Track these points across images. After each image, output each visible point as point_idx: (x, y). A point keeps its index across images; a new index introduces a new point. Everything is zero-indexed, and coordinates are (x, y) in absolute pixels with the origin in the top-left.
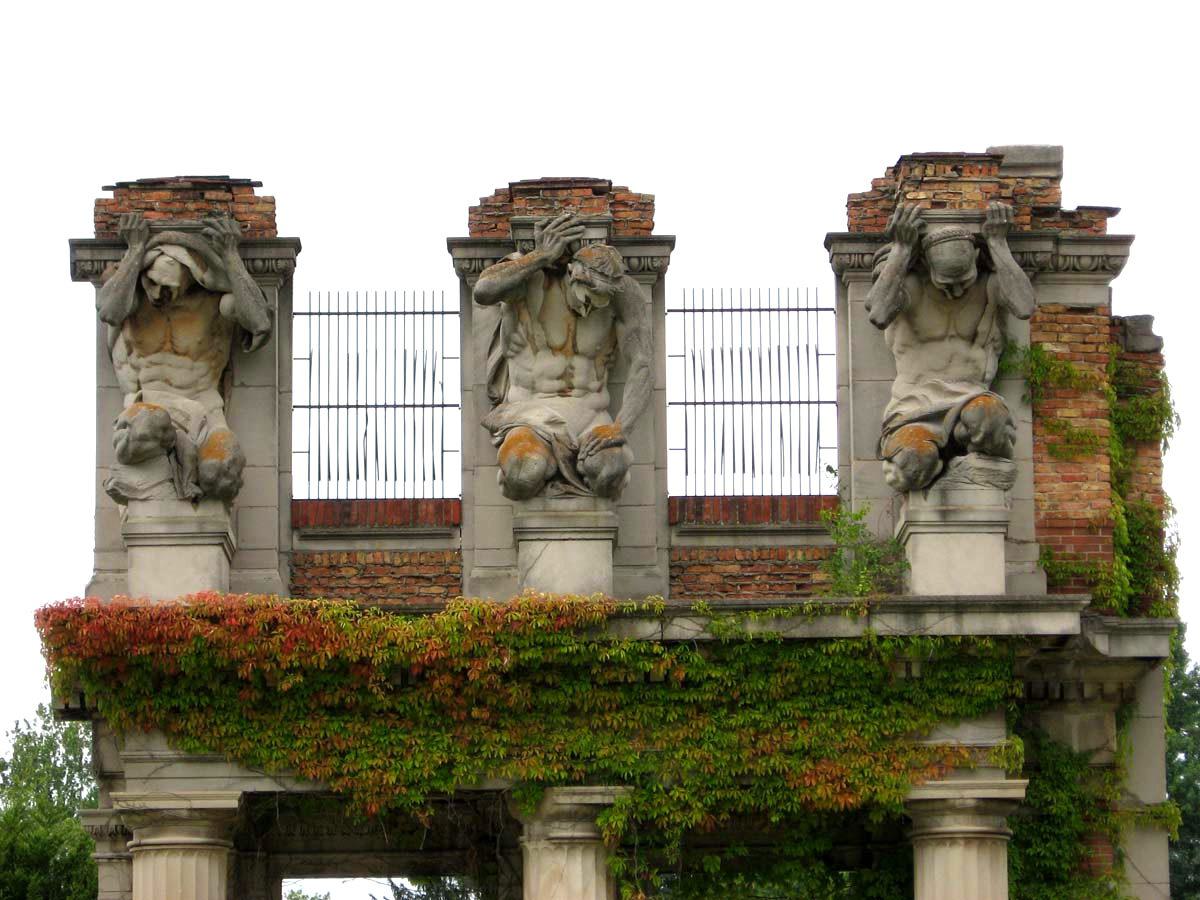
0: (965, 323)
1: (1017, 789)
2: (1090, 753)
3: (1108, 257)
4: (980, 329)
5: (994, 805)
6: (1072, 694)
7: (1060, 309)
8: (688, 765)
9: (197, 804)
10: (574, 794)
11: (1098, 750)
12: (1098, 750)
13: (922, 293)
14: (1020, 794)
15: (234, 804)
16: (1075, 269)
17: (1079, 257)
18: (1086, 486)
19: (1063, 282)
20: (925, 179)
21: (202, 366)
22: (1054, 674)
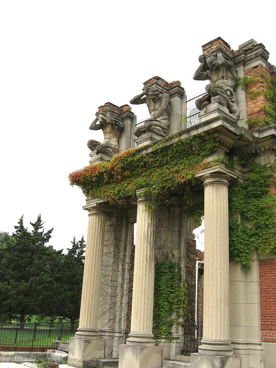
0: (220, 76)
2: (266, 165)
3: (257, 53)
4: (223, 75)
5: (214, 174)
6: (259, 152)
7: (251, 69)
8: (156, 179)
9: (92, 206)
10: (139, 191)
11: (268, 164)
12: (268, 164)
13: (212, 73)
15: (95, 205)
16: (252, 59)
17: (252, 56)
18: (258, 103)
19: (249, 64)
20: (215, 54)
21: (111, 135)
22: (251, 147)
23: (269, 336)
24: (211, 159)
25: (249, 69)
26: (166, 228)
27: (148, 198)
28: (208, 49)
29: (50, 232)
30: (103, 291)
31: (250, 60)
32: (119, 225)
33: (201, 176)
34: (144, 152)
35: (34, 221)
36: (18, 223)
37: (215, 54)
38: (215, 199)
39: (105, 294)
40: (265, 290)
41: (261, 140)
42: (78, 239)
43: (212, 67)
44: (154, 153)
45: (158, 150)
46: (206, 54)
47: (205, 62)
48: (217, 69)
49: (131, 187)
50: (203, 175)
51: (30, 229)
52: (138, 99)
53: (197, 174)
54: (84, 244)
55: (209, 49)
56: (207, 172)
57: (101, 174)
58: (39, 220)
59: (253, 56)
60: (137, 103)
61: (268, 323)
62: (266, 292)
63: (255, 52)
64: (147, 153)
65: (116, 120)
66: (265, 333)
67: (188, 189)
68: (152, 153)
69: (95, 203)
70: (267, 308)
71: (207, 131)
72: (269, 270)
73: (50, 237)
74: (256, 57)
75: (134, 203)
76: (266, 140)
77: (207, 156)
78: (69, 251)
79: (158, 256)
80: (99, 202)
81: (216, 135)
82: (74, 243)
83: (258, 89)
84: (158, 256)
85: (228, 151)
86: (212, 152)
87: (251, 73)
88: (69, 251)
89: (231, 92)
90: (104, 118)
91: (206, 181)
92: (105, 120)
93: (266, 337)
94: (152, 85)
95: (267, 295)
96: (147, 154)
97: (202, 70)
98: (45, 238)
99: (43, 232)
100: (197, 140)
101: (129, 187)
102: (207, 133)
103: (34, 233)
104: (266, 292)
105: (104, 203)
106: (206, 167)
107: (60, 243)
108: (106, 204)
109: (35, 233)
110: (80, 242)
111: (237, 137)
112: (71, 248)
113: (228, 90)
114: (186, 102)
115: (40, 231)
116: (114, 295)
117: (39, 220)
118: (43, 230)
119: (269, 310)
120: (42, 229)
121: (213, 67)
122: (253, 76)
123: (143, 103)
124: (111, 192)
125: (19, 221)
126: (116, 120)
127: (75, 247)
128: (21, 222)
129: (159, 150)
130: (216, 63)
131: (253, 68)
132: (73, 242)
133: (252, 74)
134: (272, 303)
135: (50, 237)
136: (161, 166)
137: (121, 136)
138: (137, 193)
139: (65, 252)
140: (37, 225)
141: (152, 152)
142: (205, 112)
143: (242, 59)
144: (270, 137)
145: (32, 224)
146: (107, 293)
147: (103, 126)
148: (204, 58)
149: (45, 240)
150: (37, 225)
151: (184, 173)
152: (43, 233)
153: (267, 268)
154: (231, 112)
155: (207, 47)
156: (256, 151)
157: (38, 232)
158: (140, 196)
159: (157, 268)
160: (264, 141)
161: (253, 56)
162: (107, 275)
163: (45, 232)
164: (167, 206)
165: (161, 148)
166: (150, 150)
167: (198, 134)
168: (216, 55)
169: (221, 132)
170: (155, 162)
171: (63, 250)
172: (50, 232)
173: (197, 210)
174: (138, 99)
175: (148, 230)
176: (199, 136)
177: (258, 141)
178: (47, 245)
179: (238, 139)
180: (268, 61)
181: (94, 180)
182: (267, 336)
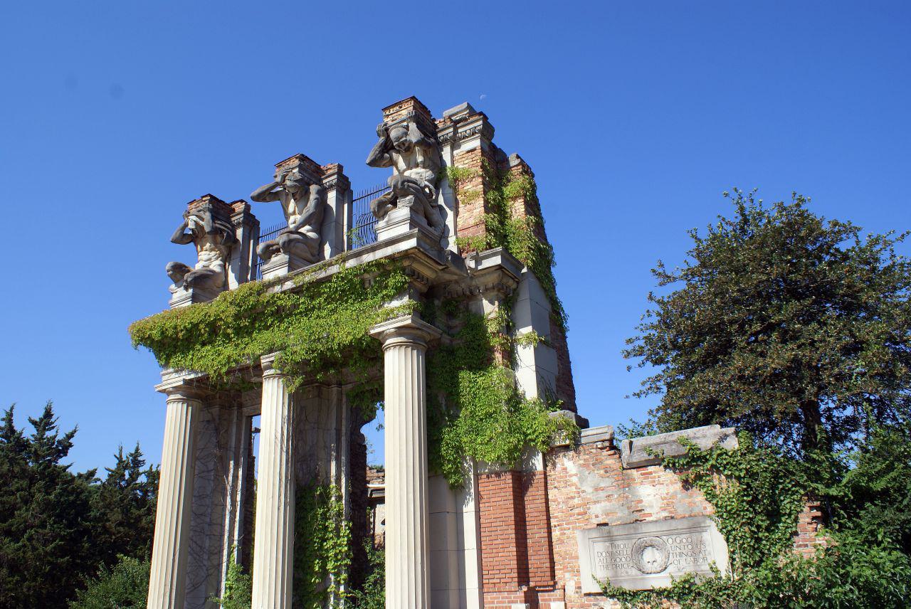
1: (407, 321)
3: (475, 127)
5: (403, 331)
8: (297, 338)
14: (409, 322)
17: (466, 131)
18: (475, 211)
20: (405, 124)
23: (498, 602)
24: (395, 304)
25: (461, 153)
26: (315, 423)
27: (286, 373)
28: (393, 115)
29: (71, 436)
30: (194, 545)
31: (464, 138)
32: (225, 420)
33: (380, 333)
34: (277, 289)
35: (38, 415)
36: (3, 419)
37: (405, 124)
38: (401, 373)
39: (198, 549)
40: (489, 525)
41: (481, 273)
42: (128, 450)
43: (399, 146)
44: (296, 291)
45: (302, 286)
46: (390, 123)
47: (388, 136)
48: (409, 150)
49: (254, 348)
50: (383, 332)
51: (29, 432)
52: (267, 193)
53: (373, 328)
54: (140, 458)
55: (396, 114)
56: (389, 327)
57: (195, 326)
58: (48, 414)
59: (468, 132)
60: (264, 200)
61: (495, 581)
62: (490, 529)
63: (471, 126)
64: (283, 289)
65: (223, 227)
66: (491, 598)
67: (356, 355)
68: (293, 291)
69: (182, 378)
70: (493, 555)
71: (391, 255)
72: (494, 492)
73: (71, 445)
74: (473, 135)
75: (254, 380)
76: (488, 273)
77: (391, 298)
78: (110, 473)
79: (301, 475)
80: (188, 377)
81: (406, 263)
82: (120, 459)
83: (475, 188)
84: (301, 475)
85: (425, 289)
86: (399, 292)
87: (464, 159)
88: (110, 473)
89: (430, 190)
90: (201, 223)
91: (388, 342)
92: (202, 227)
93: (491, 605)
94: (293, 169)
95: (493, 533)
96: (284, 292)
97: (383, 150)
98: (60, 448)
99: (55, 436)
100: (374, 269)
101: (253, 347)
102: (392, 258)
103: (36, 439)
104: (490, 529)
105: (198, 380)
106: (388, 316)
107: (89, 459)
108: (201, 382)
109: (40, 439)
110: (131, 455)
111: (441, 268)
112: (113, 466)
113: (426, 186)
114: (352, 203)
115: (49, 434)
116: (216, 551)
117: (48, 414)
118: (57, 432)
119: (496, 559)
120: (55, 430)
121: (402, 146)
122: (467, 165)
123: (274, 199)
124: (211, 360)
125: (5, 417)
126: (223, 227)
127: (122, 465)
128: (9, 418)
129: (305, 286)
130: (406, 140)
131: (468, 152)
132: (118, 456)
133: (466, 162)
134: (501, 546)
135: (71, 445)
136: (307, 312)
137: (230, 257)
138: (262, 361)
139: (103, 476)
140: (45, 422)
141: (293, 289)
142: (387, 222)
143: (450, 135)
144: (497, 267)
145: (34, 423)
146: (201, 547)
147: (197, 237)
148: (387, 130)
149: (60, 452)
150: (45, 422)
151: (343, 326)
152: (57, 439)
153: (491, 488)
154: (430, 224)
155: (392, 112)
156: (471, 292)
157: (45, 436)
158: (269, 367)
159: (299, 495)
160: (485, 274)
161: (468, 132)
162: (201, 515)
163: (60, 437)
164: (317, 384)
165: (309, 283)
166: (289, 285)
167: (376, 260)
168: (408, 126)
169: (414, 258)
170: (295, 306)
171: (96, 470)
172: (71, 436)
173: (370, 395)
174: (267, 193)
175: (282, 428)
176: (378, 264)
177: (475, 274)
178: (62, 462)
179: (442, 270)
180: (493, 141)
181: (180, 335)
182: (493, 603)
